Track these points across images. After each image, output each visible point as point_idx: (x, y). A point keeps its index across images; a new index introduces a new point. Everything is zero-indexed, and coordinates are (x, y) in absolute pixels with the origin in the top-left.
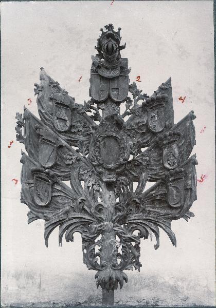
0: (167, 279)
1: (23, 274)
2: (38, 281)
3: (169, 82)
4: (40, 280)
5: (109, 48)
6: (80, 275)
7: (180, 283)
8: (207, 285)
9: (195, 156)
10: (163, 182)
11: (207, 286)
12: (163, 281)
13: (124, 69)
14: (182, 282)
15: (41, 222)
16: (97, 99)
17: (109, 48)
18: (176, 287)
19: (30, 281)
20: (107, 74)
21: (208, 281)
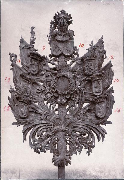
0: (92, 172)
1: (9, 172)
2: (18, 175)
3: (112, 123)
4: (19, 174)
5: (61, 24)
6: (42, 171)
7: (99, 174)
8: (115, 175)
9: (112, 88)
10: (93, 103)
11: (115, 175)
12: (90, 173)
13: (70, 36)
14: (101, 174)
15: (21, 127)
16: (54, 53)
17: (61, 24)
18: (97, 176)
19: (14, 175)
20: (60, 38)
21: (115, 172)
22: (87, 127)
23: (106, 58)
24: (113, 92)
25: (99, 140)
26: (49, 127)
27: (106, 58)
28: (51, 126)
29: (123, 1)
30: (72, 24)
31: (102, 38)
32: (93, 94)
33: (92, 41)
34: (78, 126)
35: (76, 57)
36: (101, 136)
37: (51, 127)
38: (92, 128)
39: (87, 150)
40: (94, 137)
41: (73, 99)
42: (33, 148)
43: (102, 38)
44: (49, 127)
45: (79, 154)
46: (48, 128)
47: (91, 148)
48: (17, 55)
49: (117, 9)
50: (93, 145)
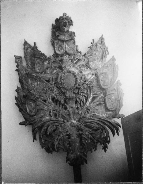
5: (61, 28)
9: (119, 80)
22: (100, 121)
23: (109, 54)
24: (120, 85)
25: (114, 134)
26: (59, 124)
27: (109, 54)
28: (61, 123)
29: (140, 4)
30: (72, 25)
31: (102, 36)
32: (88, 97)
33: (93, 40)
34: (90, 120)
35: (45, 63)
36: (115, 130)
37: (62, 124)
38: (107, 123)
39: (103, 146)
40: (108, 131)
41: (82, 94)
42: (44, 148)
43: (102, 36)
44: (59, 124)
45: (95, 151)
46: (58, 125)
47: (107, 143)
48: (21, 57)
49: (3, 3)
50: (108, 140)
